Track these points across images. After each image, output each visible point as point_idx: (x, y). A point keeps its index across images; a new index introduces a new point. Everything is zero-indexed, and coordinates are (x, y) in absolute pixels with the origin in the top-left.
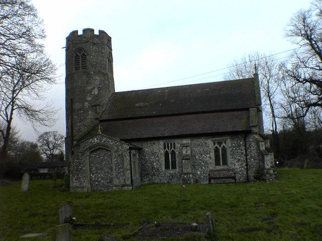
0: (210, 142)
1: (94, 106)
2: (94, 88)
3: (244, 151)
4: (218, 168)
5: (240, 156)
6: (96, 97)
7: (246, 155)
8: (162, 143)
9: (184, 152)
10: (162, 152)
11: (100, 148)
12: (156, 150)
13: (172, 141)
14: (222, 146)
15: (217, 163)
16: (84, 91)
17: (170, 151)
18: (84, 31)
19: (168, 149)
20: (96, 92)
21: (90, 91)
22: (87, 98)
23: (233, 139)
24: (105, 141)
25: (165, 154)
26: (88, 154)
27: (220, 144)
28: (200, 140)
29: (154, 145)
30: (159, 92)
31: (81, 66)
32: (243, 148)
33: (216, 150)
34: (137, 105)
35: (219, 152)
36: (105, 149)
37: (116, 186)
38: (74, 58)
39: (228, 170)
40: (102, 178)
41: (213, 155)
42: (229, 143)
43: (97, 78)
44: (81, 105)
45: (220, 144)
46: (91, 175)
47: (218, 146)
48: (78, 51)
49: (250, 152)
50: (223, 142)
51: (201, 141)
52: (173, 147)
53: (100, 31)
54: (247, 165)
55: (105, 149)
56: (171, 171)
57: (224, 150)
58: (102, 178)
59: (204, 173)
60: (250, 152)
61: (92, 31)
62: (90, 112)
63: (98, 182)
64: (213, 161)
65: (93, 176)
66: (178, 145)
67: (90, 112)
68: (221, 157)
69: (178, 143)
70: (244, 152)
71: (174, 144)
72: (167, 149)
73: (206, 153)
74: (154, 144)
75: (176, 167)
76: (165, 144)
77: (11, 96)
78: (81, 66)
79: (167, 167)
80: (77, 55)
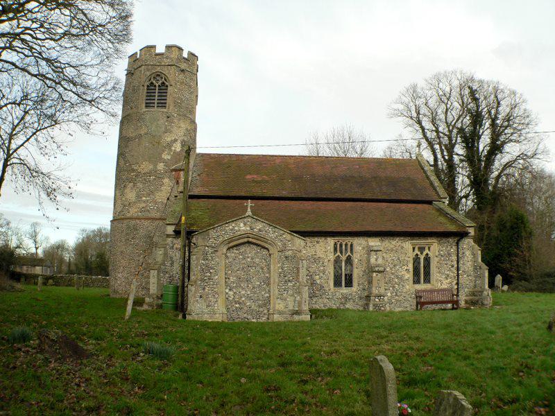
0: (407, 247)
1: (175, 170)
2: (176, 140)
3: (455, 262)
4: (418, 287)
5: (450, 270)
7: (458, 269)
8: (331, 241)
9: (373, 260)
10: (332, 257)
11: (249, 242)
12: (320, 254)
13: (349, 240)
14: (425, 253)
15: (417, 281)
16: (159, 143)
17: (344, 258)
18: (168, 47)
19: (341, 252)
21: (169, 145)
22: (163, 156)
23: (441, 245)
24: (260, 230)
25: (335, 260)
26: (225, 251)
27: (422, 249)
28: (394, 243)
29: (318, 245)
30: (277, 161)
31: (156, 101)
32: (454, 258)
34: (248, 177)
35: (419, 263)
36: (258, 245)
37: (280, 313)
38: (146, 87)
39: (432, 291)
40: (249, 298)
41: (411, 267)
42: (435, 248)
43: (182, 125)
44: (151, 167)
46: (227, 291)
47: (419, 253)
48: (154, 78)
49: (463, 264)
50: (427, 248)
51: (395, 243)
52: (349, 250)
54: (458, 284)
55: (258, 245)
56: (344, 290)
57: (427, 259)
58: (249, 298)
59: (396, 295)
60: (463, 264)
61: (181, 49)
62: (166, 181)
63: (240, 303)
64: (409, 276)
65: (231, 293)
66: (357, 248)
67: (166, 181)
68: (422, 271)
69: (359, 244)
70: (455, 263)
71: (352, 245)
72: (338, 253)
73: (402, 263)
74: (318, 242)
75: (351, 282)
76: (335, 244)
77: (9, 131)
78: (156, 101)
79: (337, 283)
80: (152, 83)
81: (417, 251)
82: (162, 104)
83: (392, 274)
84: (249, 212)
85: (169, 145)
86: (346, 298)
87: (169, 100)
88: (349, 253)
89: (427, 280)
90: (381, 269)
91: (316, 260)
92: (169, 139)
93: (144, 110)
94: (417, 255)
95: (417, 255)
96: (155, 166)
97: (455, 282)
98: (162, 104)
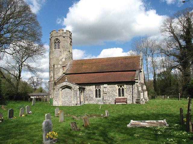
0: (116, 87)
2: (63, 58)
6: (64, 62)
15: (120, 96)
20: (64, 60)
21: (61, 60)
27: (121, 87)
30: (94, 60)
33: (119, 89)
42: (125, 86)
45: (121, 87)
47: (120, 88)
53: (67, 31)
54: (133, 97)
56: (98, 98)
57: (123, 89)
62: (61, 70)
65: (63, 100)
67: (61, 70)
72: (97, 88)
79: (96, 97)
80: (55, 42)
81: (119, 87)
82: (59, 48)
83: (112, 94)
84: (66, 80)
85: (61, 60)
86: (99, 101)
87: (60, 47)
88: (99, 88)
89: (123, 95)
90: (106, 93)
91: (90, 90)
92: (61, 58)
93: (54, 50)
94: (119, 88)
95: (119, 88)
96: (58, 66)
97: (132, 96)
98: (59, 48)
